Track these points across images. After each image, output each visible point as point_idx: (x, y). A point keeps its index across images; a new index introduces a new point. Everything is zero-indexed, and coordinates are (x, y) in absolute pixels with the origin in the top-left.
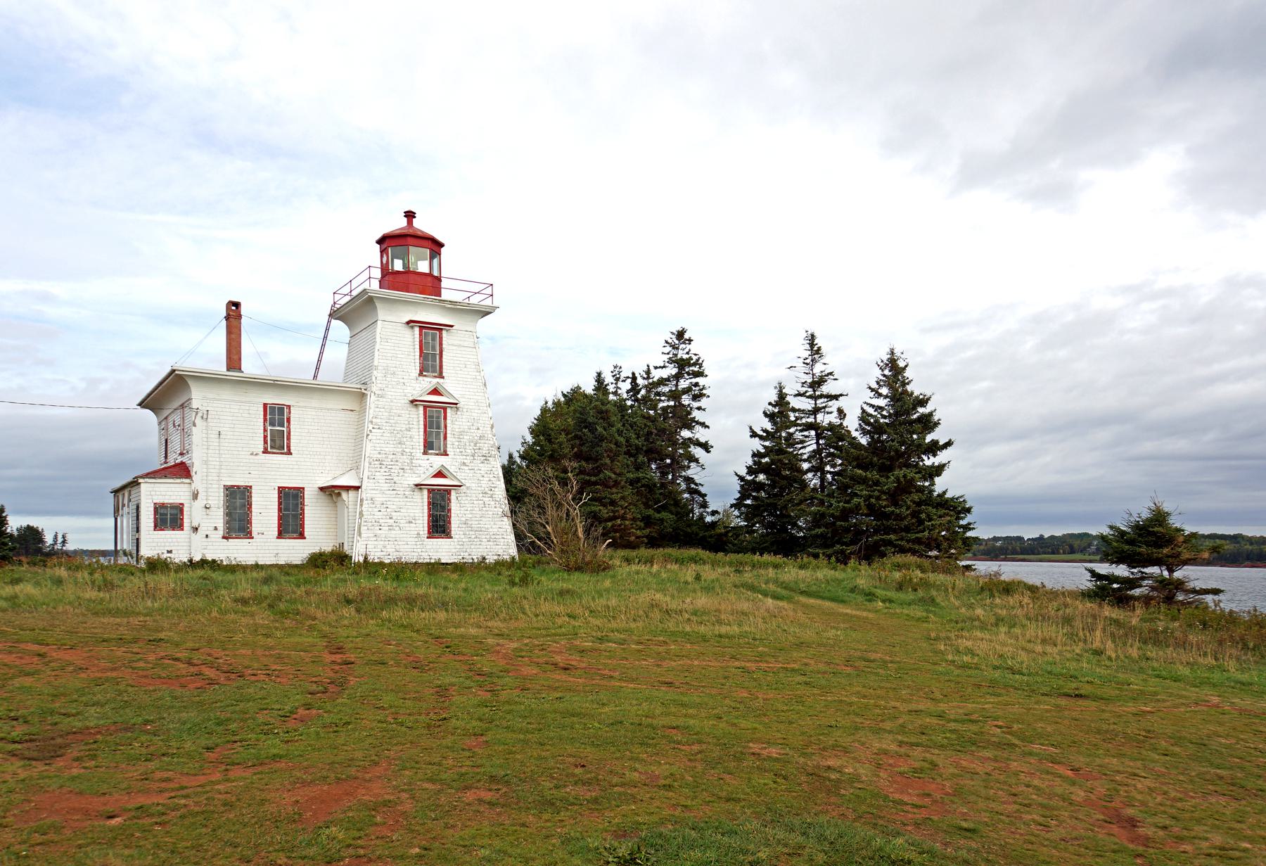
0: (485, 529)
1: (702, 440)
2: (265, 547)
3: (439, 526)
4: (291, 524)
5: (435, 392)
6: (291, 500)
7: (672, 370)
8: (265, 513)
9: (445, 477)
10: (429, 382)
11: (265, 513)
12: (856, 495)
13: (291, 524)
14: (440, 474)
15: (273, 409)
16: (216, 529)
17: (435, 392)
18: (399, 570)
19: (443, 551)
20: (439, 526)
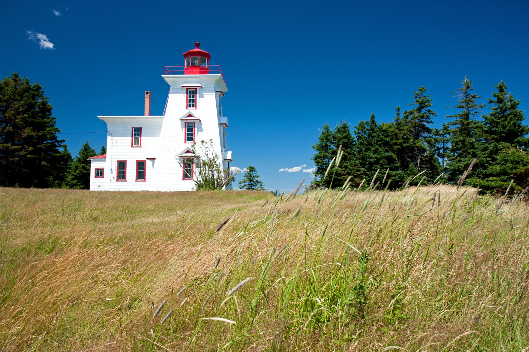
2: (131, 184)
4: (141, 175)
5: (190, 115)
6: (141, 166)
8: (131, 171)
11: (131, 171)
13: (141, 175)
15: (135, 129)
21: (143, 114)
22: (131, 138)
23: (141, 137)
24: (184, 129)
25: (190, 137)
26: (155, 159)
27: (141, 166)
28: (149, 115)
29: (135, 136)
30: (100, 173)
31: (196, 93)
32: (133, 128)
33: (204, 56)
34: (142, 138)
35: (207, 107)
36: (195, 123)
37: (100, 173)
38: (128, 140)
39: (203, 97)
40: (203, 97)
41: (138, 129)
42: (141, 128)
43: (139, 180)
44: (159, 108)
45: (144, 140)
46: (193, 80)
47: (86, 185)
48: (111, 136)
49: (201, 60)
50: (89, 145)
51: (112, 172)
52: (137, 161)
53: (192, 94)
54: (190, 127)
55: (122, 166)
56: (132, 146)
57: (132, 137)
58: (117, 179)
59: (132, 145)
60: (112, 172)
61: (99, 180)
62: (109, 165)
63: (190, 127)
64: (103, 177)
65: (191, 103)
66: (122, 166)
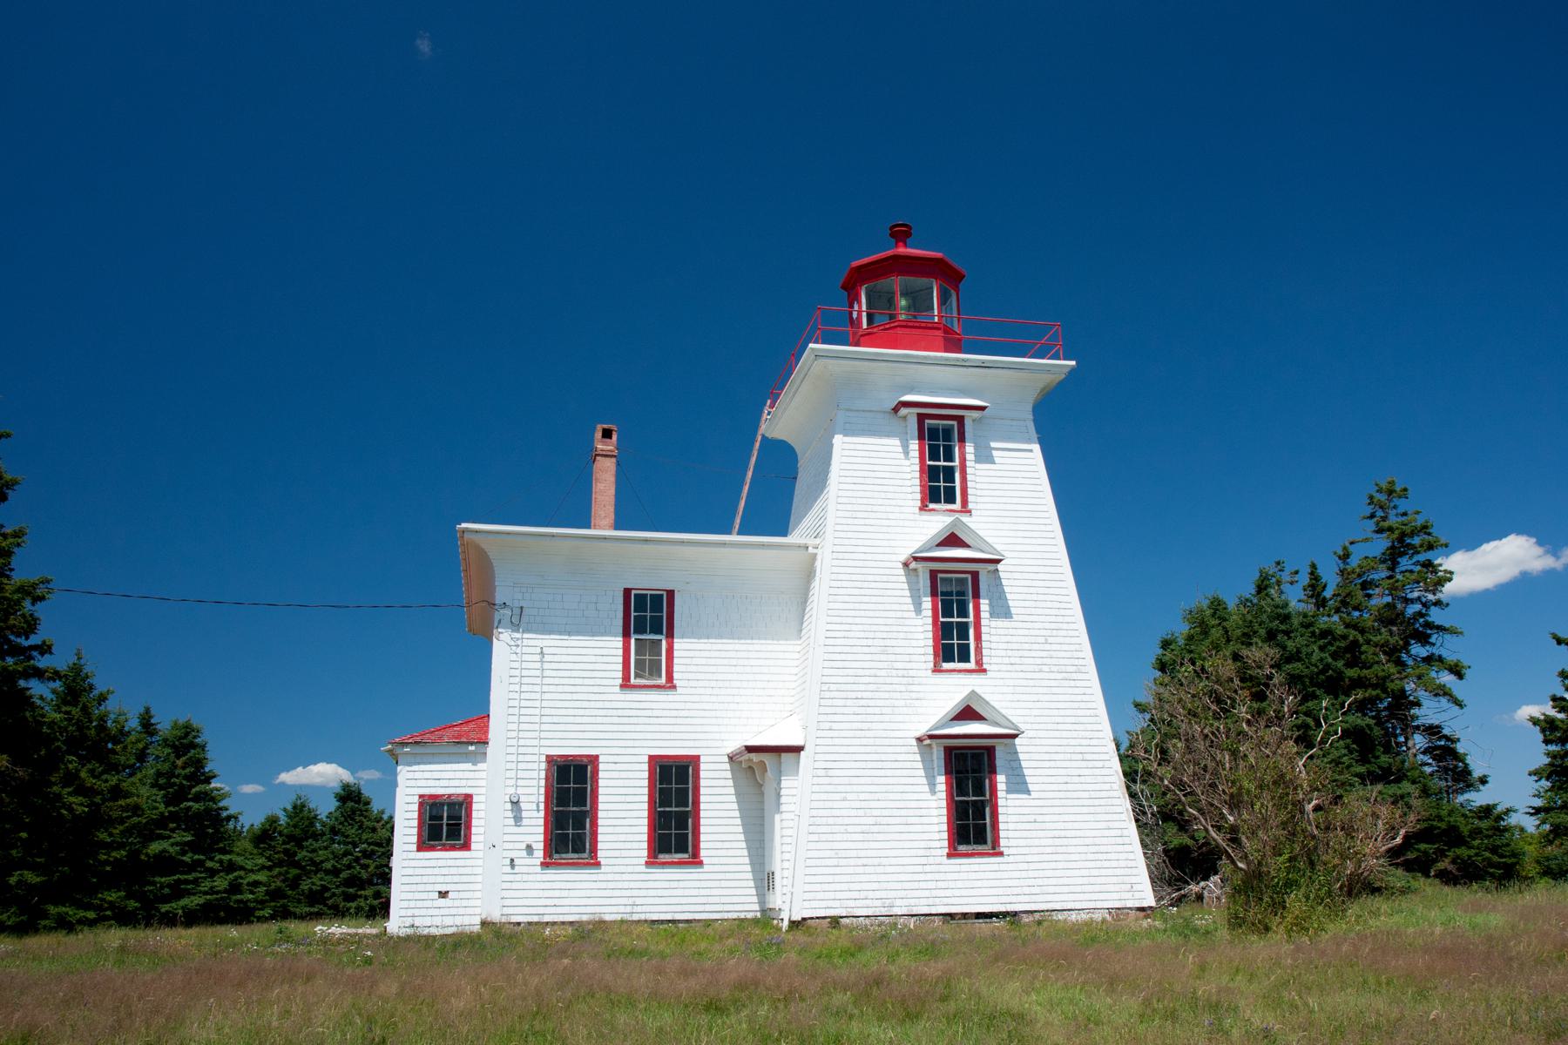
0: (1078, 847)
1: (1450, 657)
2: (624, 882)
3: (972, 827)
4: (673, 830)
5: (952, 540)
6: (673, 784)
7: (1381, 544)
8: (623, 811)
9: (978, 717)
10: (938, 521)
11: (623, 811)
12: (317, 866)
13: (673, 830)
14: (968, 713)
15: (641, 598)
16: (529, 848)
17: (952, 540)
18: (885, 935)
19: (976, 885)
20: (972, 827)
21: (583, 519)
22: (618, 642)
23: (670, 635)
24: (927, 603)
25: (953, 644)
26: (798, 750)
27: (673, 784)
28: (617, 527)
29: (639, 630)
30: (446, 824)
31: (962, 439)
32: (627, 592)
33: (949, 275)
34: (678, 644)
35: (1013, 501)
36: (975, 575)
37: (446, 824)
38: (609, 649)
39: (990, 460)
40: (990, 460)
41: (656, 600)
42: (671, 594)
43: (664, 857)
44: (771, 494)
45: (689, 652)
46: (938, 376)
47: (367, 889)
48: (515, 627)
49: (902, 284)
50: (87, 669)
51: (518, 819)
52: (550, 760)
53: (941, 441)
54: (956, 598)
55: (572, 785)
56: (626, 685)
57: (626, 634)
58: (548, 852)
59: (626, 677)
60: (518, 819)
61: (443, 860)
62: (502, 785)
63: (956, 598)
64: (466, 846)
65: (940, 486)
66: (572, 785)
